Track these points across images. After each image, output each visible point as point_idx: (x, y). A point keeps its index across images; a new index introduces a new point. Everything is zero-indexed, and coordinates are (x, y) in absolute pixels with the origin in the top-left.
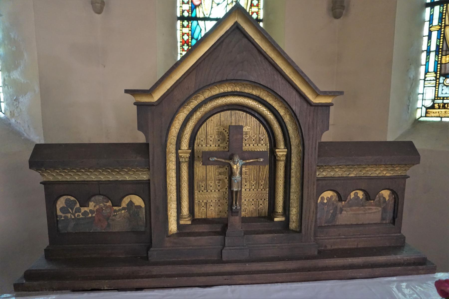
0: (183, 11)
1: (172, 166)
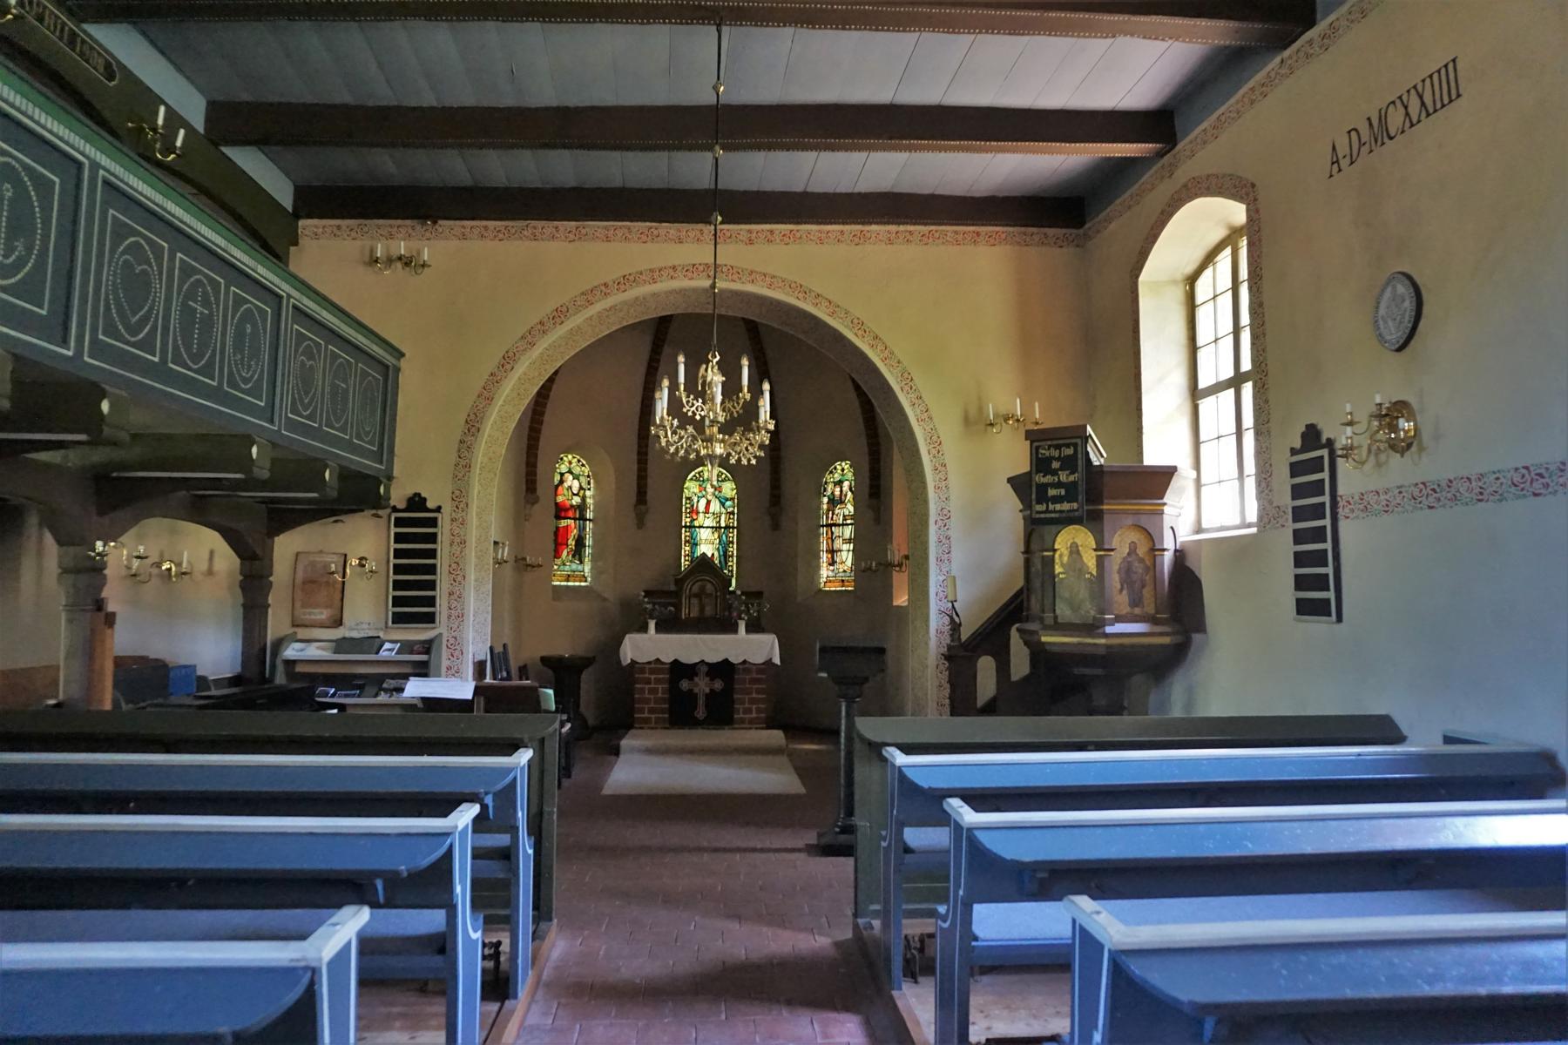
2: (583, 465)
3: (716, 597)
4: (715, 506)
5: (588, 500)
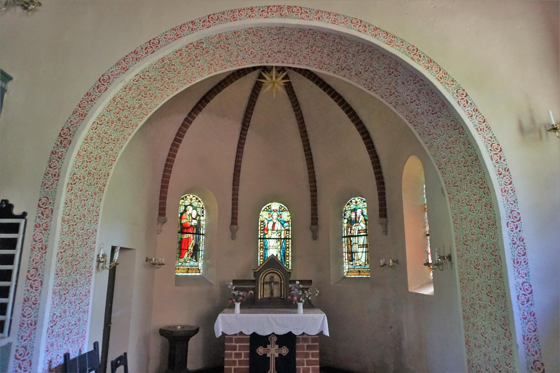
0: (261, 236)
1: (260, 285)
2: (199, 201)
3: (281, 284)
4: (278, 226)
5: (202, 222)
